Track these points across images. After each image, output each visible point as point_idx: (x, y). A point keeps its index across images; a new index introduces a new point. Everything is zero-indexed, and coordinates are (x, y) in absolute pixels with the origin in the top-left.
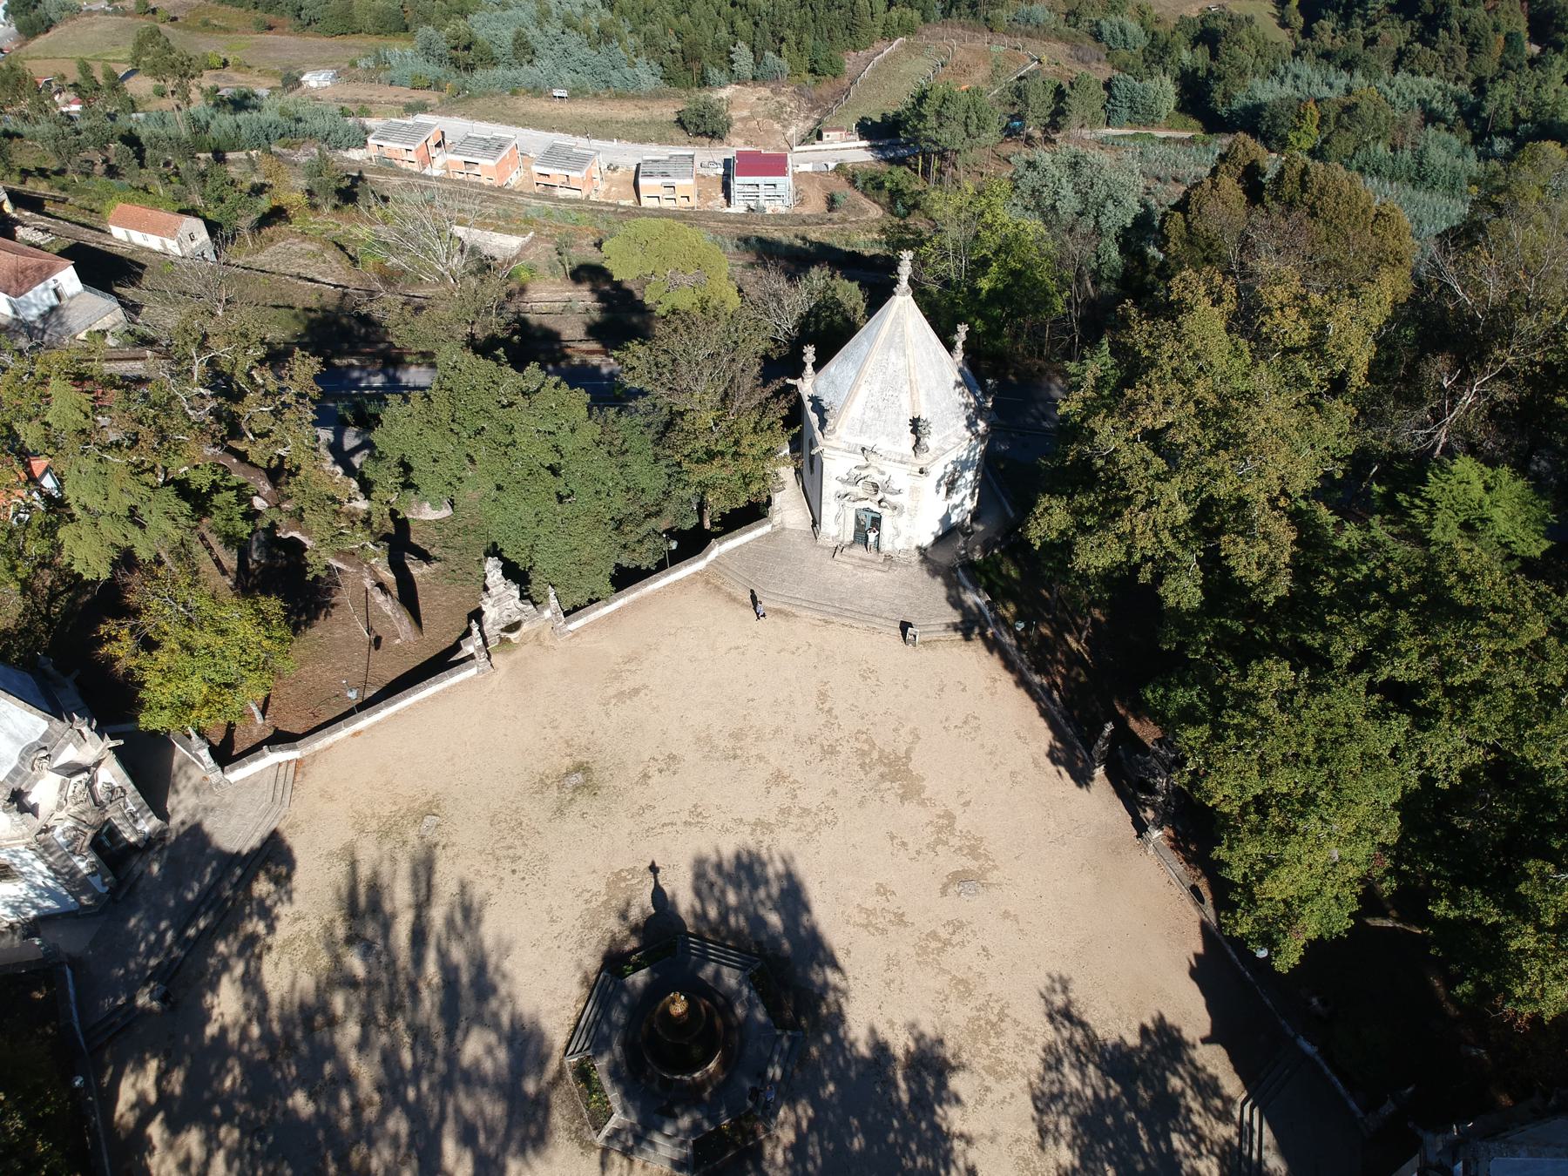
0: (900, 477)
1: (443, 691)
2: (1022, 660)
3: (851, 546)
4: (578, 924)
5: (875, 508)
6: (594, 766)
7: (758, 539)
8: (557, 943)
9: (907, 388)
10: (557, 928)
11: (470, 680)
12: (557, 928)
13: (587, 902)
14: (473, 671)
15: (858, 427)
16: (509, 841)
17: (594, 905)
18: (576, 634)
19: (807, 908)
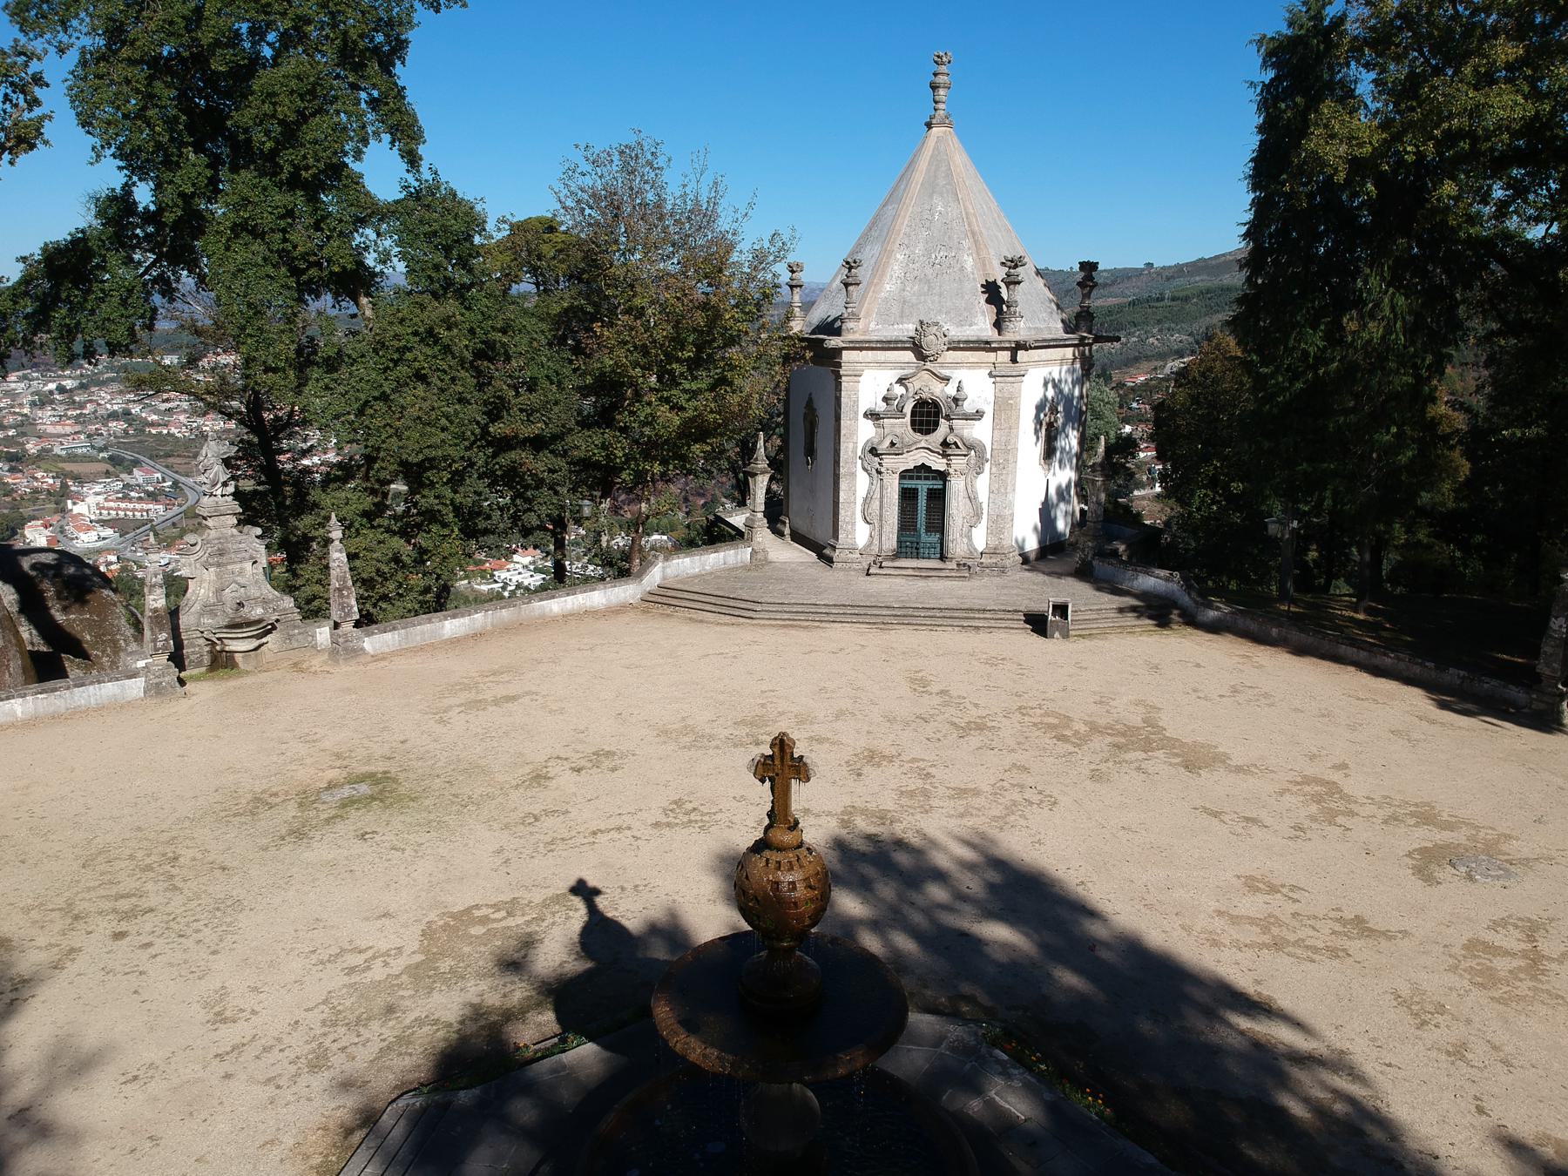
0: (973, 382)
1: (56, 717)
2: (1295, 636)
3: (897, 555)
4: (315, 1018)
5: (938, 464)
6: (402, 776)
8: (219, 1068)
9: (966, 243)
10: (229, 1035)
11: (119, 707)
12: (229, 1035)
13: (351, 970)
14: (136, 687)
15: (895, 310)
16: (129, 884)
17: (378, 972)
18: (378, 658)
19: (1085, 911)
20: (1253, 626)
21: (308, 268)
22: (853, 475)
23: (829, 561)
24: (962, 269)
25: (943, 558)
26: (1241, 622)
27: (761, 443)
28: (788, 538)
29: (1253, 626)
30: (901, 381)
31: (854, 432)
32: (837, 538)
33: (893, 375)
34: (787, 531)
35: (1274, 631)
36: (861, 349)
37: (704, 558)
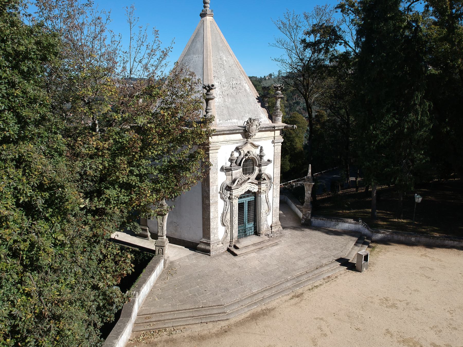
5: (255, 189)
7: (160, 278)
15: (225, 112)
20: (402, 238)
21: (38, 55)
22: (216, 202)
23: (207, 252)
24: (245, 90)
25: (257, 233)
26: (396, 237)
27: (385, 223)
28: (150, 238)
29: (402, 238)
30: (237, 149)
31: (216, 180)
32: (209, 238)
33: (234, 147)
34: (149, 234)
35: (413, 239)
36: (224, 134)
37: (150, 280)
